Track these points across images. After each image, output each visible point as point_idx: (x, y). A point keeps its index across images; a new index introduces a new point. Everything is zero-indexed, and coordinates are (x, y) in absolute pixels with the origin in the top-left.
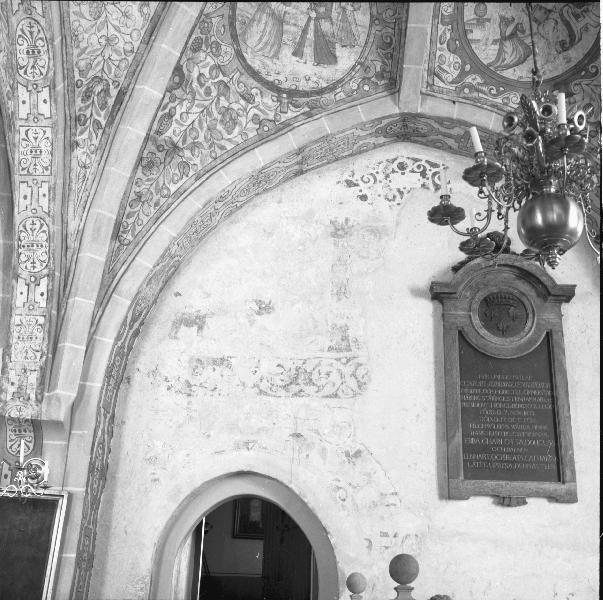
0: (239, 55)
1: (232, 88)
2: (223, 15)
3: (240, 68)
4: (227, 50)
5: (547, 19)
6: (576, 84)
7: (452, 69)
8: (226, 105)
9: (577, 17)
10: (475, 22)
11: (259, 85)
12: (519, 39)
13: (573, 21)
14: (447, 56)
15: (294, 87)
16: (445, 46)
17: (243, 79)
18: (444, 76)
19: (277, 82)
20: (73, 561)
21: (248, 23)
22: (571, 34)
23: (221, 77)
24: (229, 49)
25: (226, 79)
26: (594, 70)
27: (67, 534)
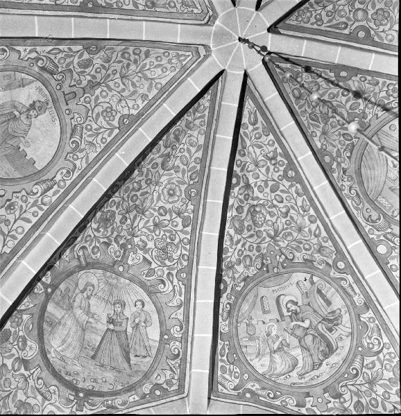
0: (44, 353)
1: (31, 382)
2: (33, 314)
3: (42, 364)
4: (33, 345)
5: (306, 335)
6: (342, 386)
7: (233, 377)
8: (23, 398)
9: (330, 330)
10: (247, 339)
11: (57, 384)
12: (286, 353)
13: (328, 334)
14: (228, 367)
15: (90, 388)
16: (225, 358)
17: (43, 375)
18: (226, 383)
19: (75, 382)
20: (96, 177)
21: (54, 324)
22: (329, 345)
23: (22, 371)
24: (34, 346)
25: (26, 373)
26: (355, 372)
27: (298, 120)
